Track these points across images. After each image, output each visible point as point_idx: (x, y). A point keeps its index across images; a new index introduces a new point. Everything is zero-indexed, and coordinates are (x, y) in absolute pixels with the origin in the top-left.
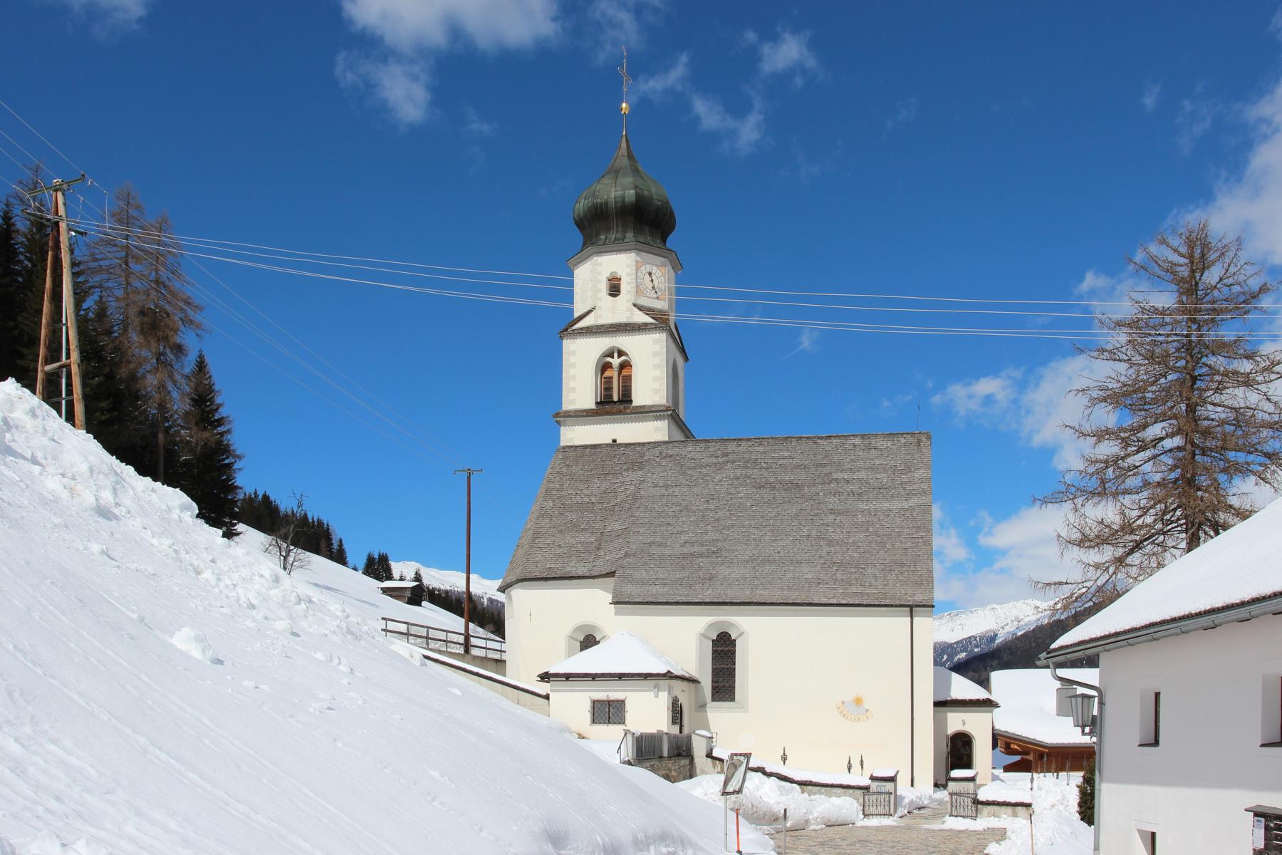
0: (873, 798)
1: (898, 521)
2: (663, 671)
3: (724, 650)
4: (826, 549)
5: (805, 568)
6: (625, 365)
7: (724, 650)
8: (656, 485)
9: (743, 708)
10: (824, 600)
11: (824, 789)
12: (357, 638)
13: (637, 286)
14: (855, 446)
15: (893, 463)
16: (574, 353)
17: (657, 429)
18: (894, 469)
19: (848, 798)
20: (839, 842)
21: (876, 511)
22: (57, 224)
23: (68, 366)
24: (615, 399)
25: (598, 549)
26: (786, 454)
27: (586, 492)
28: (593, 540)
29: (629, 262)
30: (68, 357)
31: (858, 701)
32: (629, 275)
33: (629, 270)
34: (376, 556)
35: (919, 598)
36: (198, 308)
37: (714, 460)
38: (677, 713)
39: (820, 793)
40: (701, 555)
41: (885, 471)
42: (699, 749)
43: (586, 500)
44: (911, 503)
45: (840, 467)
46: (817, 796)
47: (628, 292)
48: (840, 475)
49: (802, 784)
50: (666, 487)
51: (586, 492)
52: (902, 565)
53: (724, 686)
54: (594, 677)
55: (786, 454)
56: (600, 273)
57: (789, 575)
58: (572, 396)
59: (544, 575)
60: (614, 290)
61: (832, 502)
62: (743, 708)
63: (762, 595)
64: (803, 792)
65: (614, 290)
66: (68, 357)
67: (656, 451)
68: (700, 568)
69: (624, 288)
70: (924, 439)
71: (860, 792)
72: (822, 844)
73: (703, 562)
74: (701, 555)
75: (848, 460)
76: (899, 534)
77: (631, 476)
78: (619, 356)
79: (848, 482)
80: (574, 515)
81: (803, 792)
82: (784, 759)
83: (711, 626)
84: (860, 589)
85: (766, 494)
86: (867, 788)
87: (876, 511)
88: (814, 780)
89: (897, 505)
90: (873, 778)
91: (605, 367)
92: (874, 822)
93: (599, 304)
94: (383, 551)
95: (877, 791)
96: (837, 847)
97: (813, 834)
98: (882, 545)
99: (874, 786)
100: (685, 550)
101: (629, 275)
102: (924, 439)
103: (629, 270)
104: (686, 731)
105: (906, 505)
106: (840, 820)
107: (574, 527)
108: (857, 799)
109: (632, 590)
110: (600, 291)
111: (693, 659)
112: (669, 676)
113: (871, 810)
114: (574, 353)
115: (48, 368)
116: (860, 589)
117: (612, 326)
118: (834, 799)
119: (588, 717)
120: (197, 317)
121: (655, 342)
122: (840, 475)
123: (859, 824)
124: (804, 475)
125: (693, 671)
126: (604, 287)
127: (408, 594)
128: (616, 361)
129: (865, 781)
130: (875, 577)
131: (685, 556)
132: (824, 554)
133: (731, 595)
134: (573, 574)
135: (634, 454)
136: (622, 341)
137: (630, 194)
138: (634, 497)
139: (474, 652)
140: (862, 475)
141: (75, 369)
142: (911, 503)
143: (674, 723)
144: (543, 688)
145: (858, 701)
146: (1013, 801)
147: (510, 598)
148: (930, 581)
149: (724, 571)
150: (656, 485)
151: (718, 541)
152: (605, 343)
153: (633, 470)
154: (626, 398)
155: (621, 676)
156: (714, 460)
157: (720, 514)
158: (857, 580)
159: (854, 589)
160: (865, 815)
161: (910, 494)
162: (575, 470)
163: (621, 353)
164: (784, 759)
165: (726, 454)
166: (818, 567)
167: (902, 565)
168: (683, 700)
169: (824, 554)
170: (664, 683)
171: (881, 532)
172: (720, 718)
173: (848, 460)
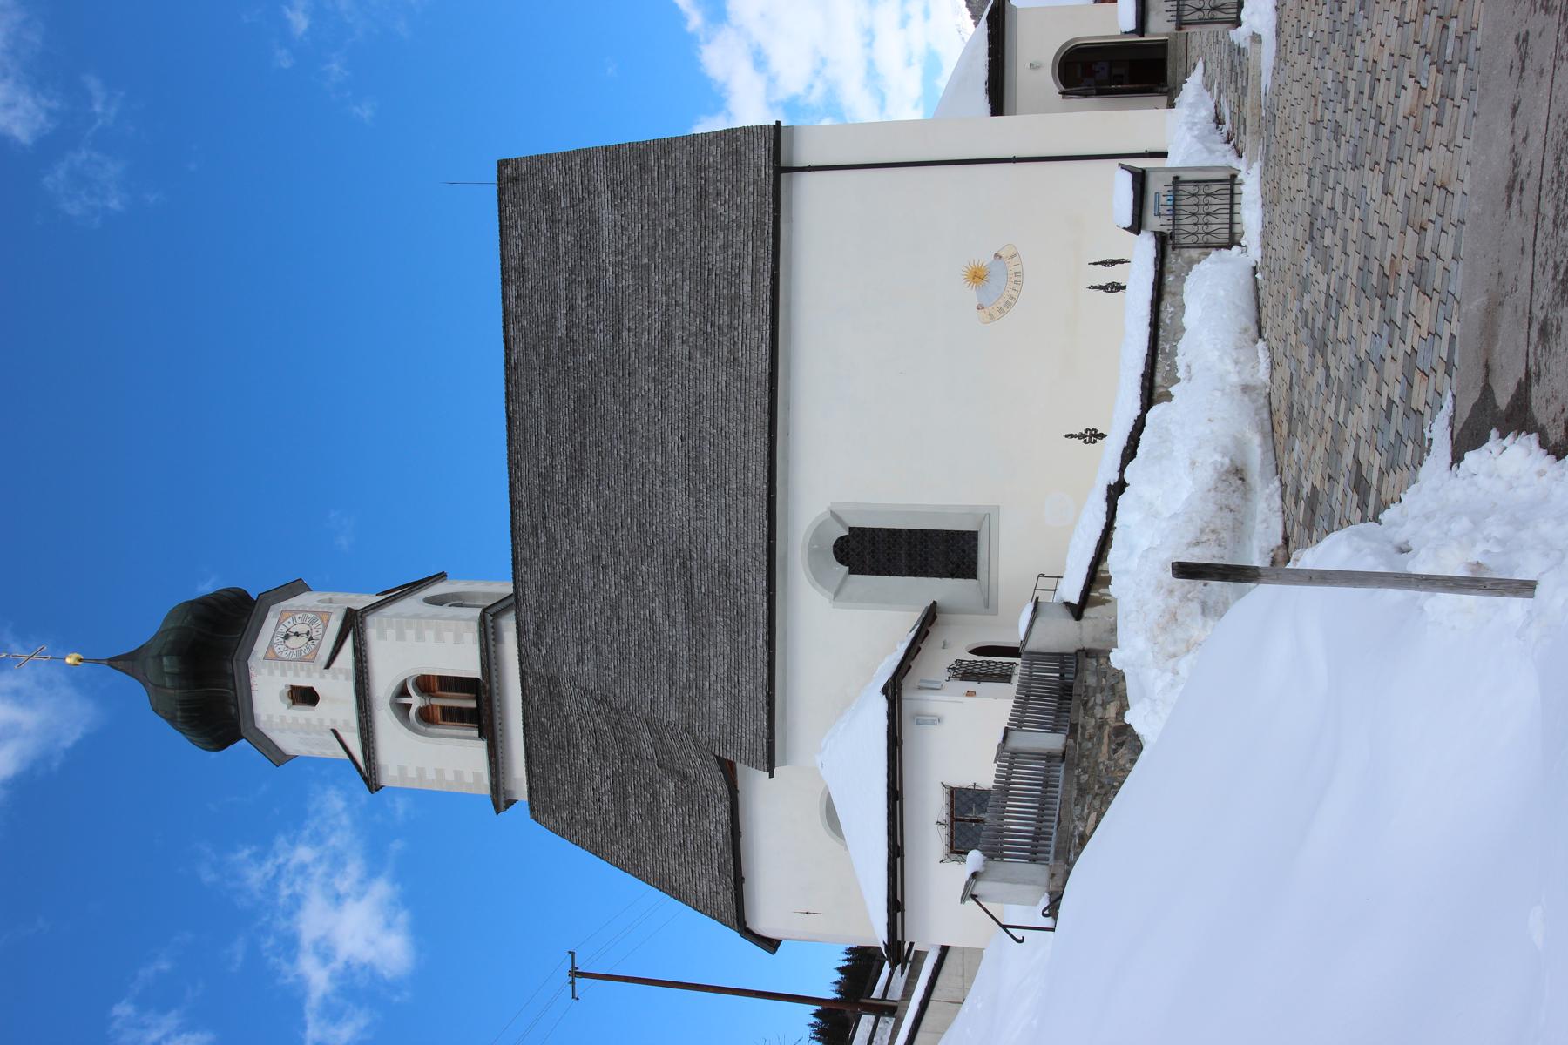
0: (1187, 225)
1: (632, 208)
2: (882, 704)
3: (870, 551)
4: (678, 348)
5: (708, 388)
6: (425, 684)
7: (870, 551)
8: (581, 660)
9: (988, 516)
10: (764, 349)
11: (1164, 346)
13: (302, 660)
14: (518, 297)
15: (543, 225)
16: (402, 769)
18: (553, 222)
19: (1187, 287)
20: (1316, 294)
21: (615, 253)
24: (473, 704)
25: (685, 777)
26: (531, 422)
27: (596, 783)
28: (671, 785)
29: (265, 671)
31: (978, 276)
32: (284, 674)
33: (277, 673)
35: (762, 156)
37: (542, 550)
38: (987, 664)
39: (1173, 353)
40: (689, 591)
41: (554, 239)
42: (1058, 634)
43: (608, 784)
44: (603, 187)
45: (550, 323)
46: (1180, 361)
47: (309, 675)
48: (562, 322)
49: (1150, 394)
50: (582, 641)
51: (596, 783)
52: (703, 194)
53: (948, 552)
54: (896, 851)
55: (531, 422)
56: (283, 718)
57: (721, 420)
58: (469, 779)
59: (730, 881)
60: (305, 696)
61: (601, 337)
62: (988, 516)
63: (755, 474)
64: (1168, 397)
65: (305, 696)
67: (533, 651)
68: (710, 592)
69: (303, 682)
70: (507, 171)
71: (1172, 259)
72: (1320, 346)
73: (700, 583)
74: (689, 591)
75: (538, 307)
76: (653, 204)
77: (570, 705)
78: (408, 695)
79: (572, 308)
80: (633, 810)
81: (1168, 397)
82: (1093, 436)
83: (818, 577)
84: (746, 276)
85: (592, 459)
86: (1164, 242)
87: (615, 253)
88: (1140, 368)
89: (606, 214)
90: (1137, 226)
91: (425, 716)
92: (1251, 216)
93: (329, 725)
95: (1177, 217)
97: (1283, 372)
98: (671, 236)
99: (1155, 222)
100: (681, 618)
101: (284, 674)
102: (507, 171)
103: (277, 673)
105: (606, 196)
106: (1245, 302)
107: (651, 812)
108: (1191, 263)
109: (750, 728)
110: (308, 720)
111: (879, 617)
112: (893, 691)
113: (1218, 225)
114: (402, 769)
116: (746, 276)
117: (359, 707)
118: (1191, 318)
121: (382, 636)
122: (562, 322)
123: (1254, 253)
124: (561, 388)
125: (904, 624)
126: (303, 713)
128: (416, 701)
129: (1143, 249)
130: (723, 248)
131: (691, 620)
132: (685, 350)
133: (755, 535)
134: (727, 829)
137: (1484, 299)
138: (600, 700)
140: (561, 280)
142: (603, 187)
145: (978, 276)
146: (1145, 331)
148: (732, 135)
149: (714, 549)
150: (581, 660)
151: (665, 556)
152: (385, 719)
153: (560, 695)
155: (895, 794)
156: (542, 550)
157: (622, 546)
158: (729, 284)
159: (746, 289)
160: (1232, 241)
161: (590, 191)
162: (564, 795)
163: (403, 692)
164: (1093, 436)
165: (534, 527)
166: (708, 361)
167: (703, 194)
168: (960, 651)
169: (685, 350)
170: (911, 700)
171: (648, 241)
172: (1010, 561)
173: (538, 307)
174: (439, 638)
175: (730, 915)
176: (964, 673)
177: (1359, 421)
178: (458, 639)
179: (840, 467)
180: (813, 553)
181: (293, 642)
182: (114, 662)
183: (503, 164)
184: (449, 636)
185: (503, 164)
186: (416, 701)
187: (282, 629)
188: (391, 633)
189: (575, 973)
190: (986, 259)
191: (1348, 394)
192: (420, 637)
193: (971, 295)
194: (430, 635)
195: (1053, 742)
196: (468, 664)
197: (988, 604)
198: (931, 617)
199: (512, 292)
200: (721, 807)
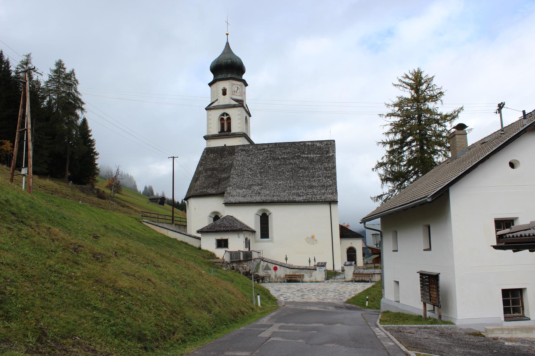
3: (264, 219)
6: (229, 119)
7: (264, 219)
12: (105, 226)
17: (240, 141)
22: (25, 83)
23: (27, 130)
24: (225, 130)
30: (27, 127)
31: (313, 237)
34: (148, 187)
36: (83, 103)
38: (248, 243)
42: (255, 255)
48: (304, 156)
53: (265, 233)
60: (224, 93)
65: (224, 93)
66: (27, 127)
69: (228, 92)
82: (286, 259)
91: (222, 119)
94: (150, 185)
96: (303, 291)
104: (251, 250)
115: (20, 130)
119: (229, 241)
120: (83, 106)
122: (304, 156)
126: (221, 92)
127: (159, 201)
128: (225, 118)
135: (232, 150)
136: (227, 111)
139: (174, 222)
141: (29, 131)
143: (246, 247)
144: (199, 235)
145: (313, 237)
147: (188, 202)
152: (221, 111)
154: (229, 129)
163: (227, 115)
174: (239, 123)
175: (192, 193)
176: (246, 239)
177: (288, 294)
178: (239, 127)
179: (279, 215)
180: (264, 210)
181: (236, 89)
182: (227, 44)
183: (334, 141)
184: (240, 125)
185: (334, 141)
186: (225, 118)
187: (238, 86)
188: (239, 113)
189: (173, 157)
190: (316, 238)
191: (292, 293)
192: (239, 119)
193: (310, 236)
194: (239, 121)
195: (242, 259)
196: (234, 130)
197: (256, 241)
198: (254, 232)
199: (310, 144)
200: (214, 192)
